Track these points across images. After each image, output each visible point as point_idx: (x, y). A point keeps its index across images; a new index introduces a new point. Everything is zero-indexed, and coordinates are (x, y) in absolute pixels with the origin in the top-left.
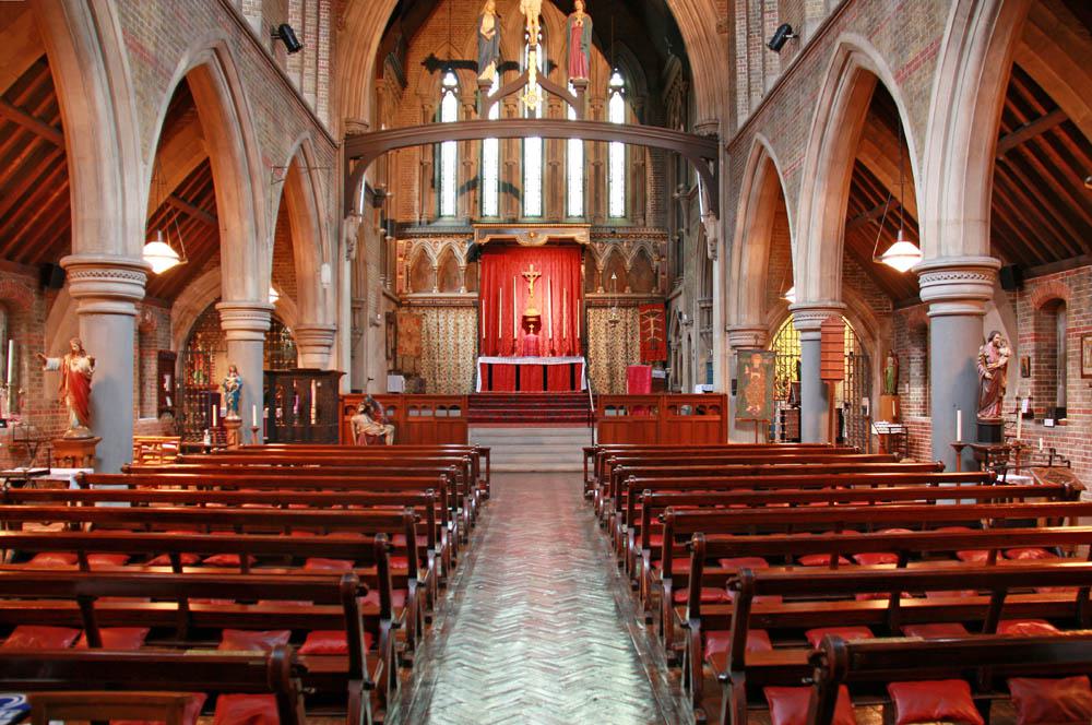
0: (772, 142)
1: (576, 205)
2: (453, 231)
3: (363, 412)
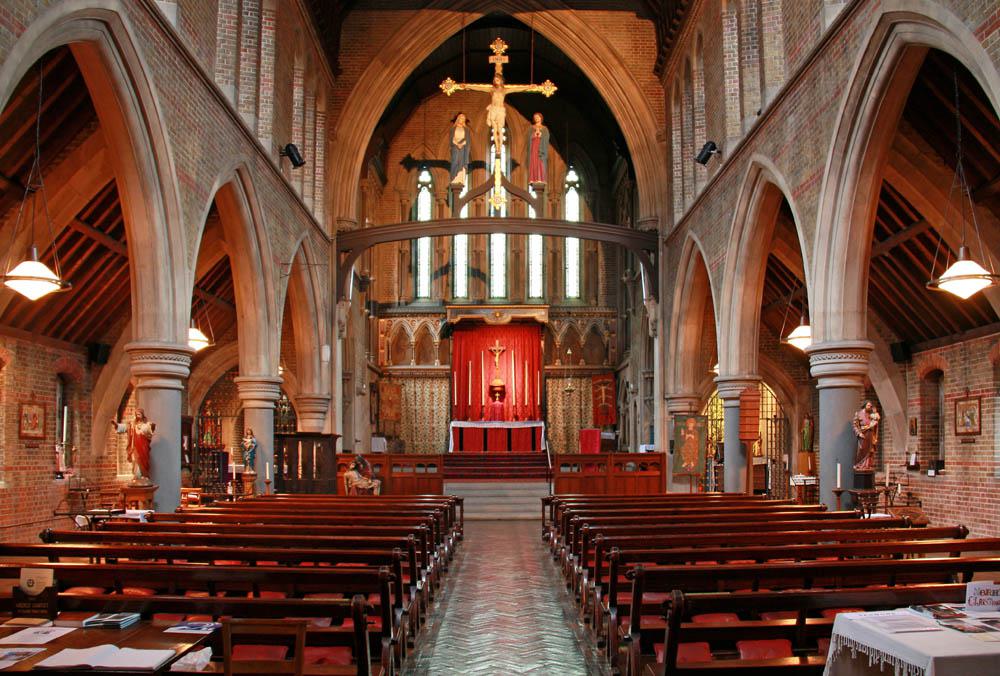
0: (701, 239)
1: (536, 288)
2: (428, 311)
3: (353, 469)
